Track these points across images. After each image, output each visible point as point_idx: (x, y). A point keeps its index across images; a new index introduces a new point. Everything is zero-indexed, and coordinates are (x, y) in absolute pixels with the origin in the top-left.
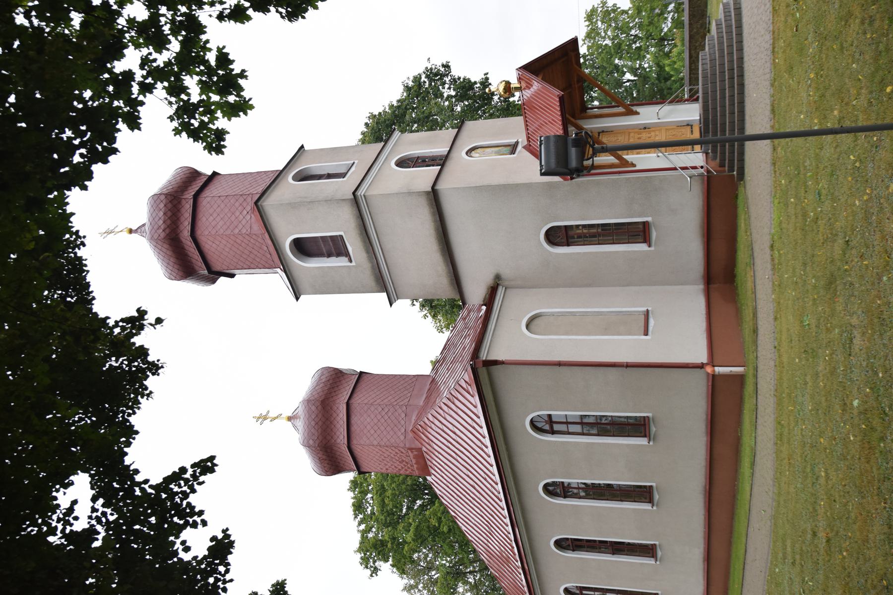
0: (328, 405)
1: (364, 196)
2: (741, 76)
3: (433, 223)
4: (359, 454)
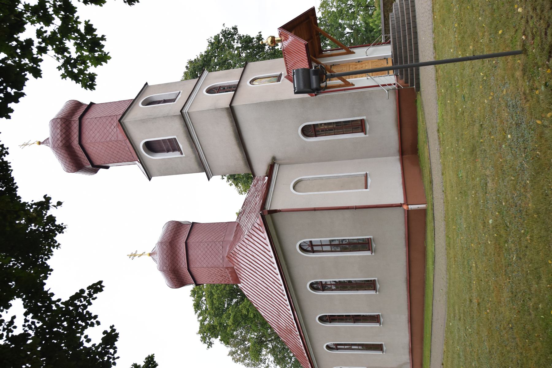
1: (187, 112)
4: (195, 273)
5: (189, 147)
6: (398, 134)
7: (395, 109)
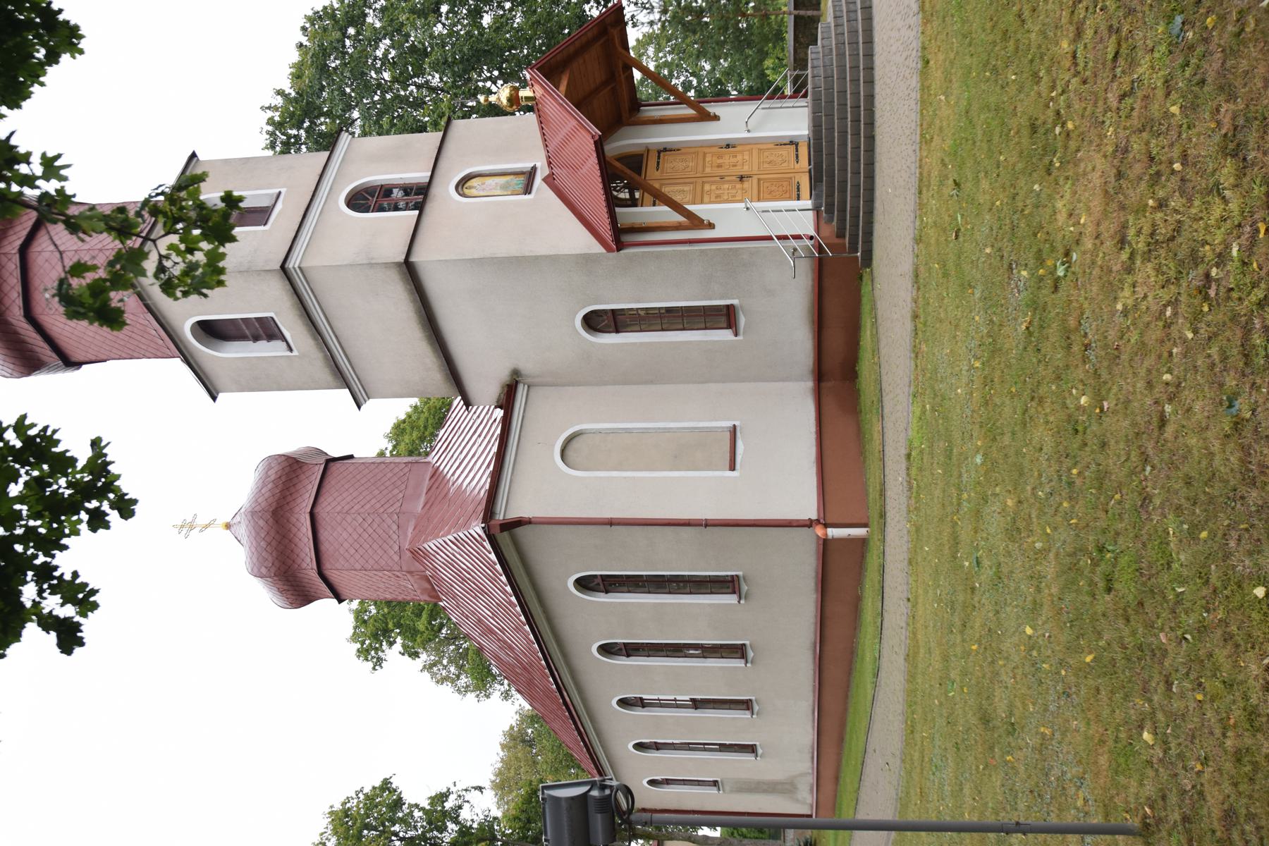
0: (282, 516)
1: (300, 268)
2: (871, 124)
3: (411, 304)
4: (336, 580)
5: (308, 336)
6: (814, 338)
7: (810, 288)
